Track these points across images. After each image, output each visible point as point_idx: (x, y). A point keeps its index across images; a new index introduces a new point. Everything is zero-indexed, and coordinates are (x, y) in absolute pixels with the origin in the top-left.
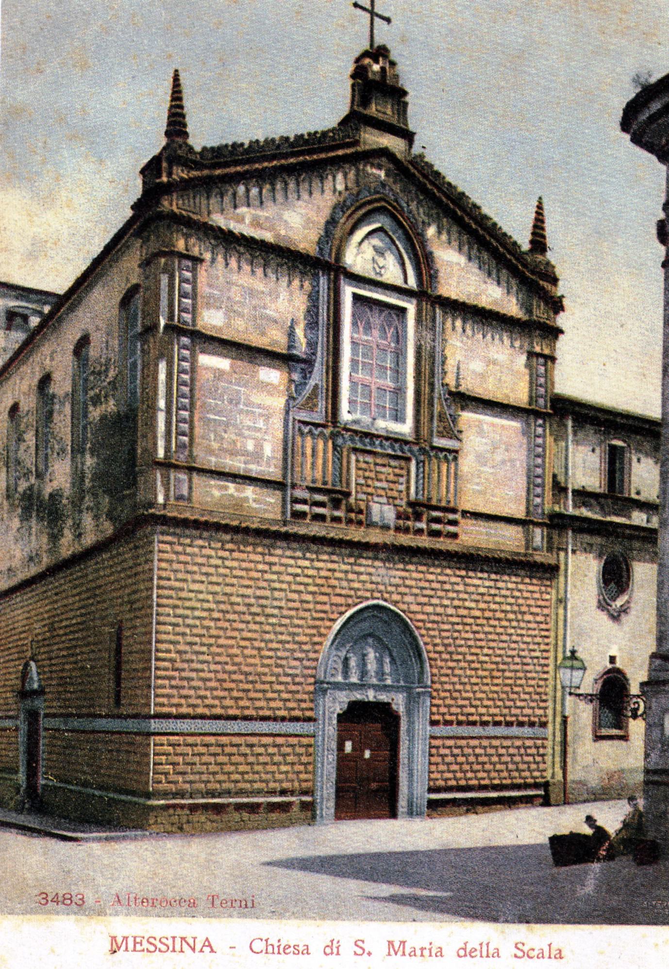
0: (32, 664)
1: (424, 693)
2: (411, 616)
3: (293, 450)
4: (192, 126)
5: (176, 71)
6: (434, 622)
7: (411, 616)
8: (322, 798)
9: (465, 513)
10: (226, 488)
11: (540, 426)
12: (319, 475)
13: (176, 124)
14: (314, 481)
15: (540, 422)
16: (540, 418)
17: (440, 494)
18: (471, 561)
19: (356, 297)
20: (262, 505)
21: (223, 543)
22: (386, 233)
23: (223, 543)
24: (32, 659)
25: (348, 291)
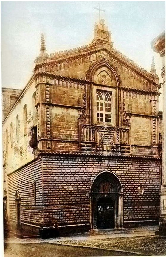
0: (18, 192)
1: (122, 195)
2: (117, 174)
3: (24, 94)
4: (47, 47)
5: (42, 33)
6: (123, 175)
7: (117, 174)
8: (140, 149)
9: (132, 146)
10: (62, 144)
11: (154, 120)
12: (88, 139)
13: (43, 49)
14: (87, 140)
15: (155, 119)
16: (155, 118)
17: (124, 140)
18: (134, 159)
19: (98, 90)
20: (73, 149)
21: (52, 158)
22: (105, 71)
23: (52, 158)
24: (18, 191)
25: (95, 88)
